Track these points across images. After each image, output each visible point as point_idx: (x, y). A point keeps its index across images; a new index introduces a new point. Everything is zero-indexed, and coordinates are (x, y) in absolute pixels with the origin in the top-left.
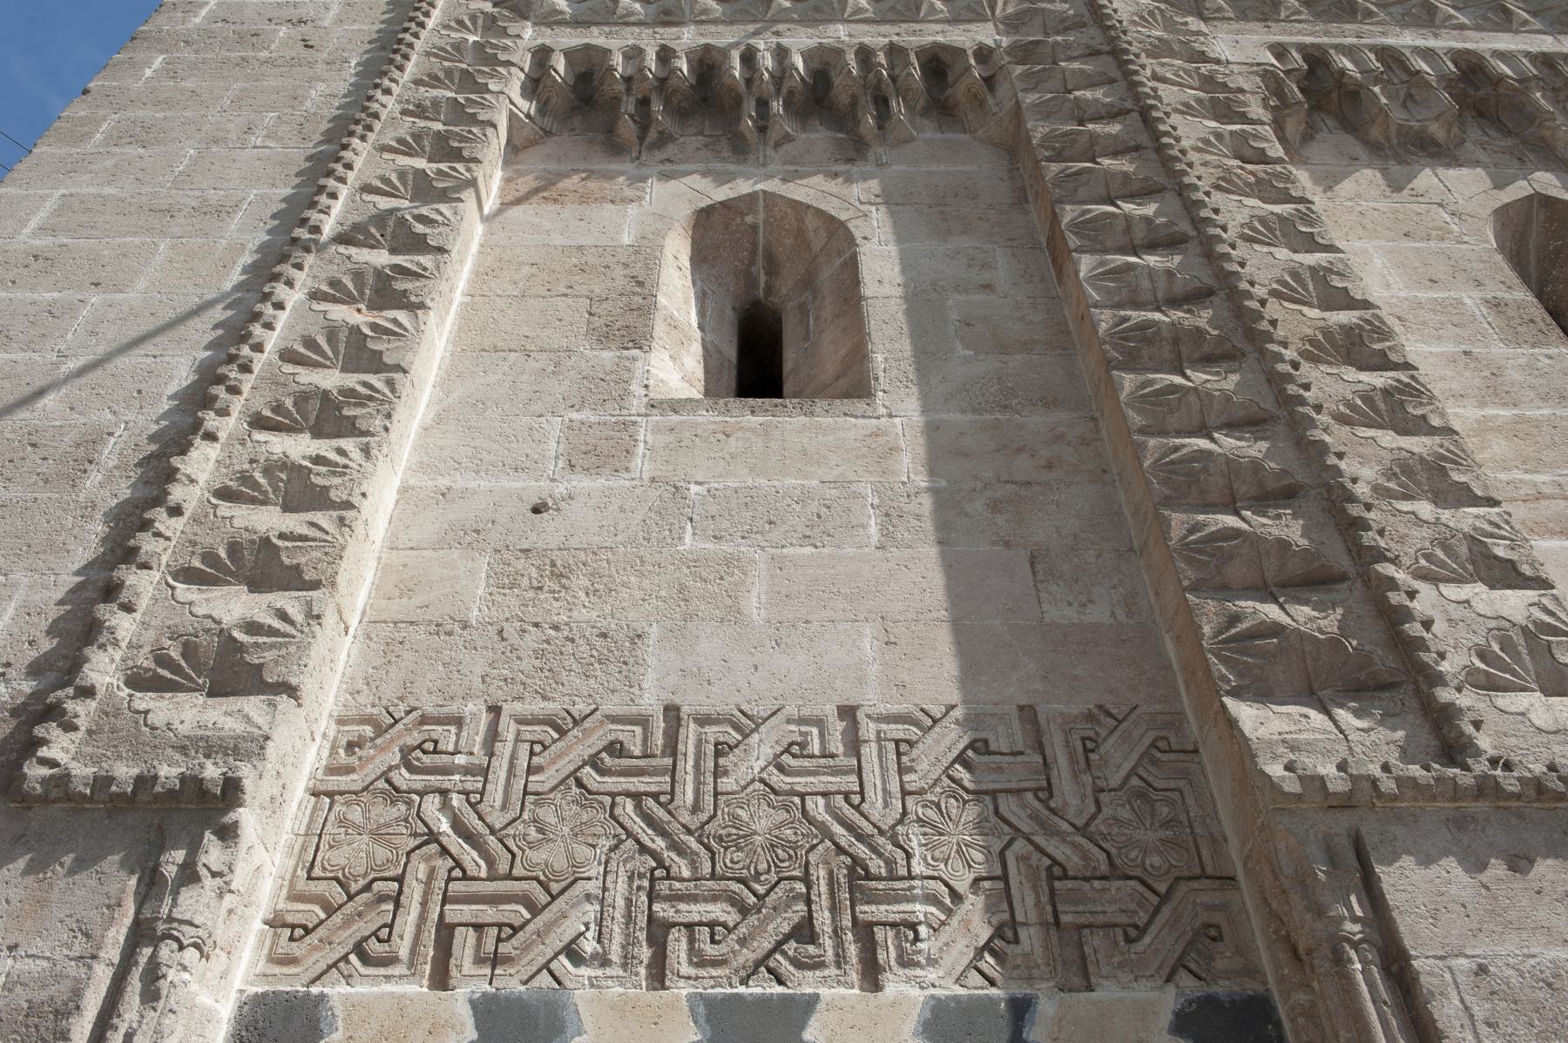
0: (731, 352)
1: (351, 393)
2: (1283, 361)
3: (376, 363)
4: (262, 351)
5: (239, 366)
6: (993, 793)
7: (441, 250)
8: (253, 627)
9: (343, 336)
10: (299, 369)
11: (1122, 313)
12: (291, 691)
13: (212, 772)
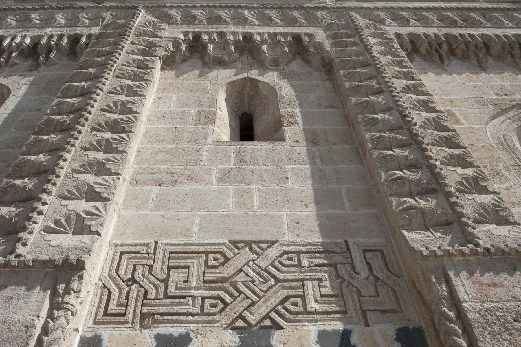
1: (115, 139)
2: (390, 83)
5: (22, 243)
7: (142, 95)
10: (114, 95)
11: (381, 151)
13: (73, 258)
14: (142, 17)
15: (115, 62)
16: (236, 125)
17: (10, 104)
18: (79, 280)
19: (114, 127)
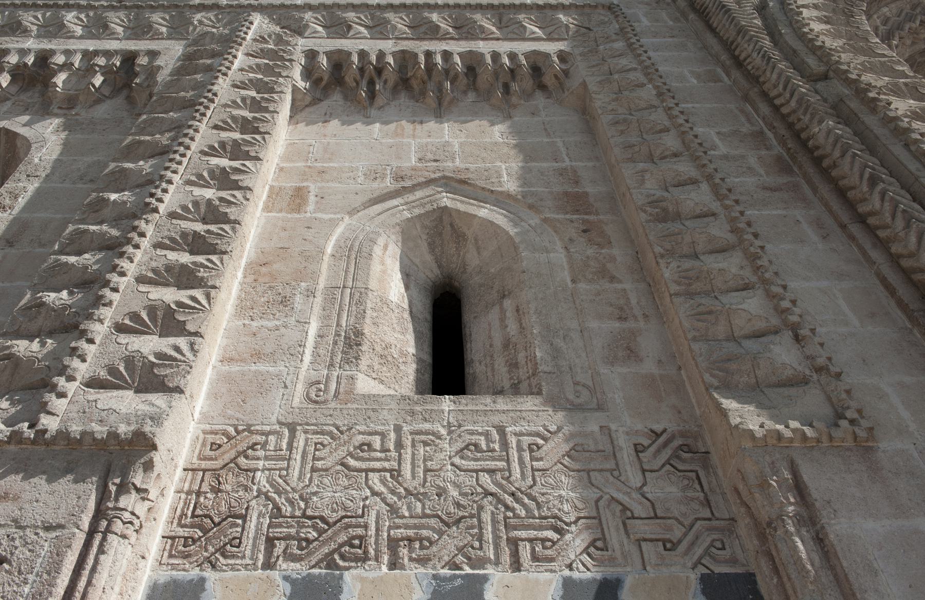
0: (428, 358)
3: (236, 186)
4: (172, 184)
6: (588, 472)
7: (257, 159)
9: (160, 314)
12: (181, 392)
14: (259, 23)
15: (188, 148)
16: (426, 314)
17: (24, 187)
18: (145, 471)
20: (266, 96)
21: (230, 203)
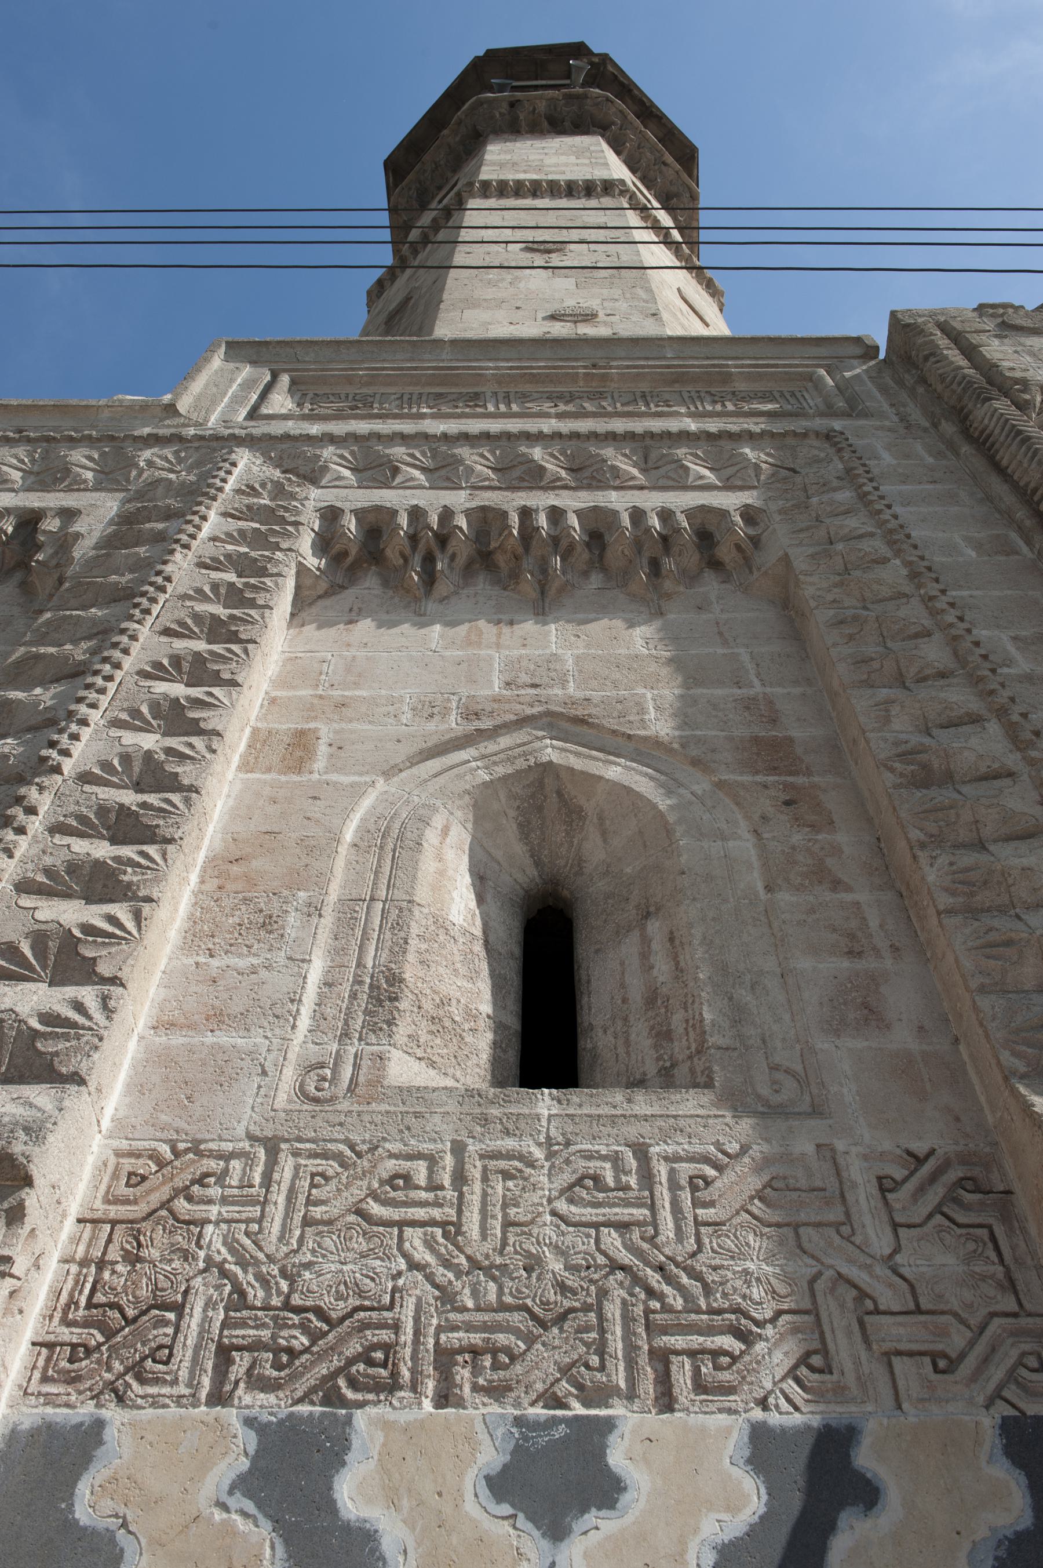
0: (514, 1023)
3: (195, 728)
6: (796, 1227)
7: (234, 683)
8: (89, 929)
9: (53, 945)
16: (512, 946)
19: (124, 826)
20: (252, 581)
21: (183, 757)
